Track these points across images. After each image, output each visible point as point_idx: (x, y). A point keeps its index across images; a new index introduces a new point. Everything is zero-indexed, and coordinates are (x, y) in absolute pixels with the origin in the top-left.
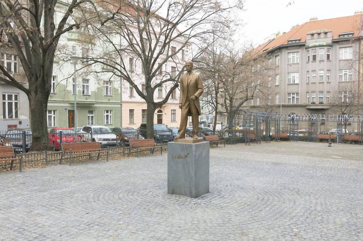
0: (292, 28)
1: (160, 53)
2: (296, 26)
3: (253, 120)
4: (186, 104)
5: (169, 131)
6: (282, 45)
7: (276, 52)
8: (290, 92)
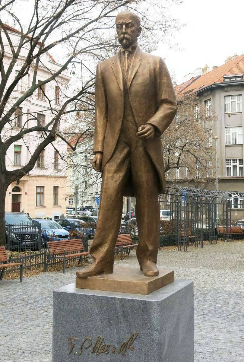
0: (227, 60)
1: (21, 74)
2: (234, 56)
3: (169, 204)
4: (117, 152)
5: (34, 227)
6: (215, 84)
7: (205, 94)
8: (236, 158)
